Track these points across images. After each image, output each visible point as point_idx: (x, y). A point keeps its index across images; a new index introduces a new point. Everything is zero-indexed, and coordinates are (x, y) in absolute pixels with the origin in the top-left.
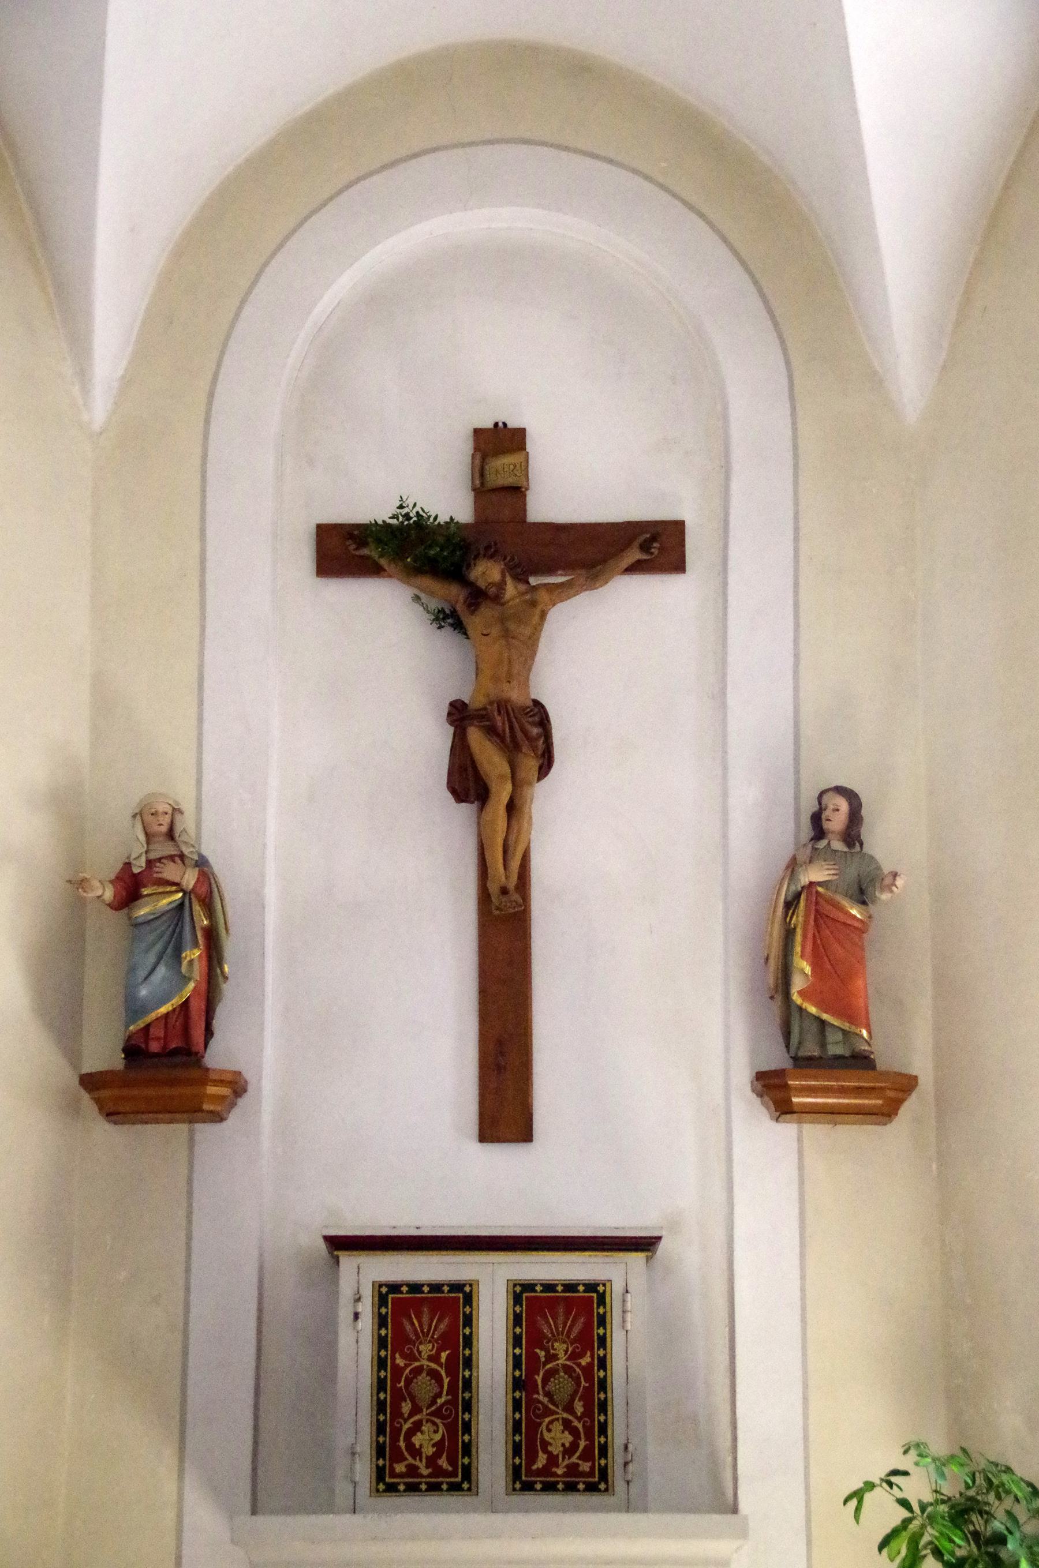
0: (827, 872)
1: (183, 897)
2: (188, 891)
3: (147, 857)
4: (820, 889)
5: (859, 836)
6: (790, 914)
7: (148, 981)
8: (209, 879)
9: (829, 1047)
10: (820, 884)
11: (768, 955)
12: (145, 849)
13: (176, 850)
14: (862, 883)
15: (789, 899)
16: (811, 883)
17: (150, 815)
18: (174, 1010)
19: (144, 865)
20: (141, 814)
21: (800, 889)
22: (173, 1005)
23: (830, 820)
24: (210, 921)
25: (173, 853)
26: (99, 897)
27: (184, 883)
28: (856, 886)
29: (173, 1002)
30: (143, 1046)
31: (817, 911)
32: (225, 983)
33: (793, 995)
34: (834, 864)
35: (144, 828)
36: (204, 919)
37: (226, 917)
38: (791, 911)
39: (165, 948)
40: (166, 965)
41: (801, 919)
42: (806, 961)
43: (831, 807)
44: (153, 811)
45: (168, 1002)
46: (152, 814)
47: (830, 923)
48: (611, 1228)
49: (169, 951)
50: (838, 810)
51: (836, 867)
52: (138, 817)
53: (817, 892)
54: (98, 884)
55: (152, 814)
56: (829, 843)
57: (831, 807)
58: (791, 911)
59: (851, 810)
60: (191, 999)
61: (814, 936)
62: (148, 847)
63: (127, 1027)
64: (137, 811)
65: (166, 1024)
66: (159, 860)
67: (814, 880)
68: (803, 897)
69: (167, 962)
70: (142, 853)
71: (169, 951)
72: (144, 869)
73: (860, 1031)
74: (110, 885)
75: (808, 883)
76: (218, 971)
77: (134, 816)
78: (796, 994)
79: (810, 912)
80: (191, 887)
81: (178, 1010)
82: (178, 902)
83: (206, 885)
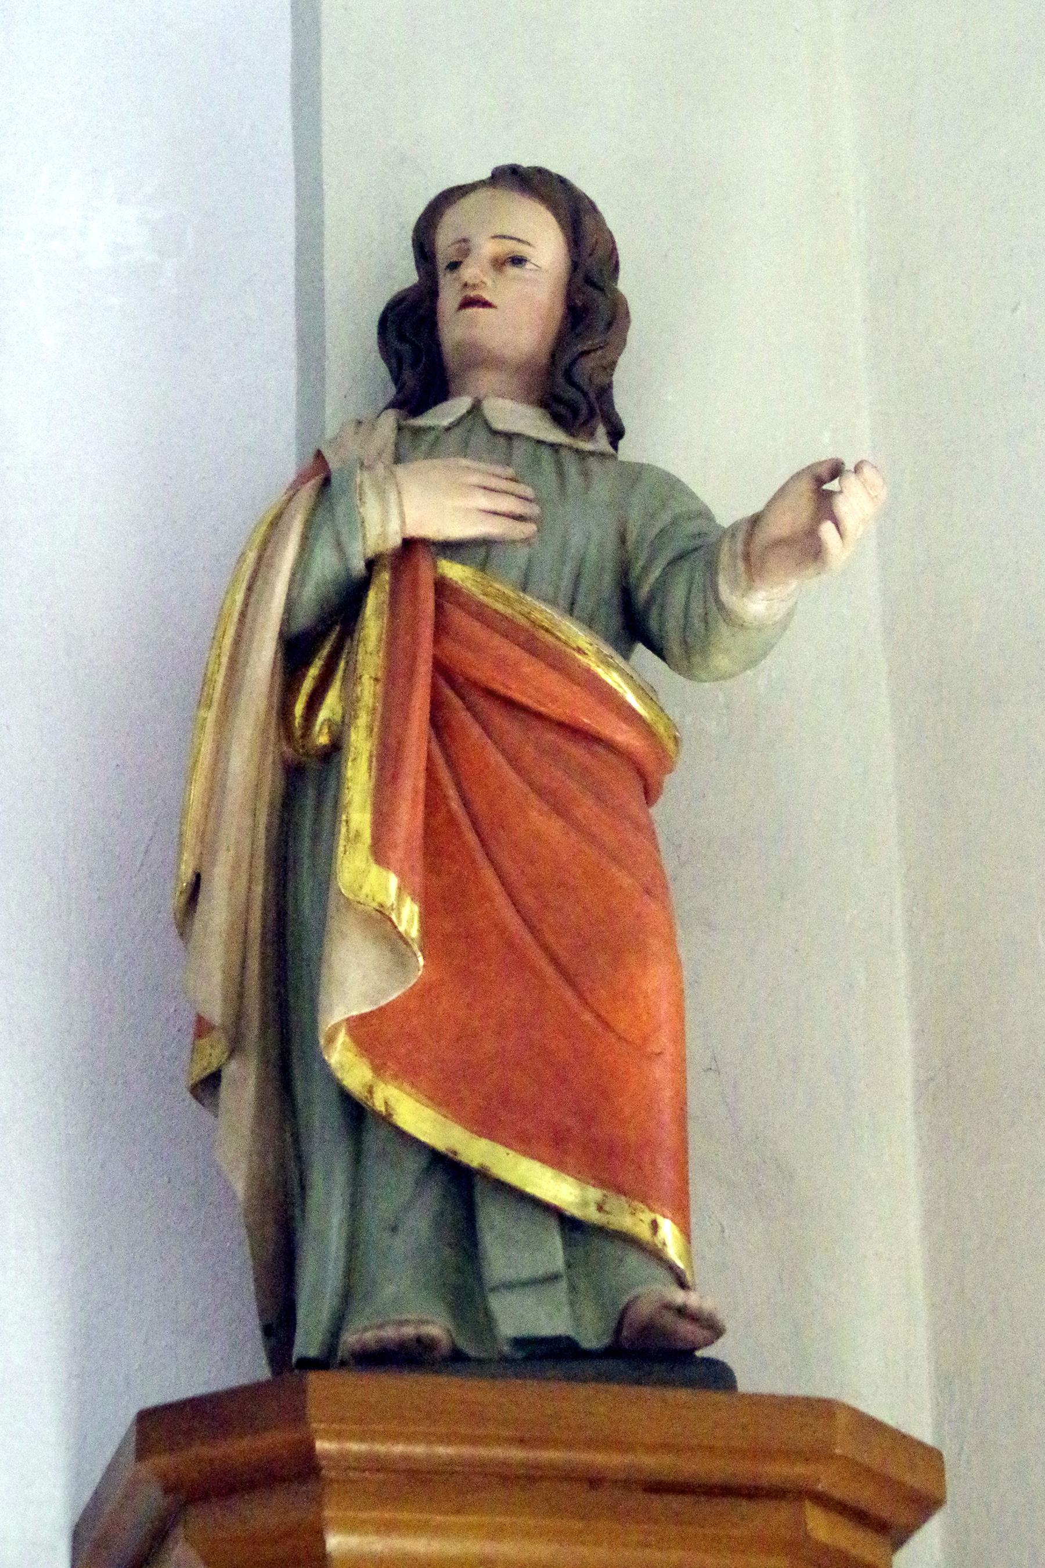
0: (485, 501)
4: (454, 571)
5: (605, 392)
6: (307, 686)
9: (497, 1304)
10: (452, 548)
11: (198, 877)
14: (632, 580)
15: (303, 620)
16: (410, 545)
21: (358, 566)
23: (486, 304)
28: (608, 579)
31: (442, 670)
33: (331, 1039)
34: (513, 480)
38: (314, 671)
41: (368, 691)
42: (400, 874)
43: (487, 248)
47: (499, 719)
48: (846, 1506)
50: (518, 261)
51: (529, 492)
53: (442, 587)
56: (476, 409)
57: (487, 248)
58: (314, 671)
59: (575, 266)
61: (430, 773)
67: (415, 530)
68: (374, 600)
73: (655, 1226)
75: (395, 541)
78: (342, 1037)
79: (411, 672)
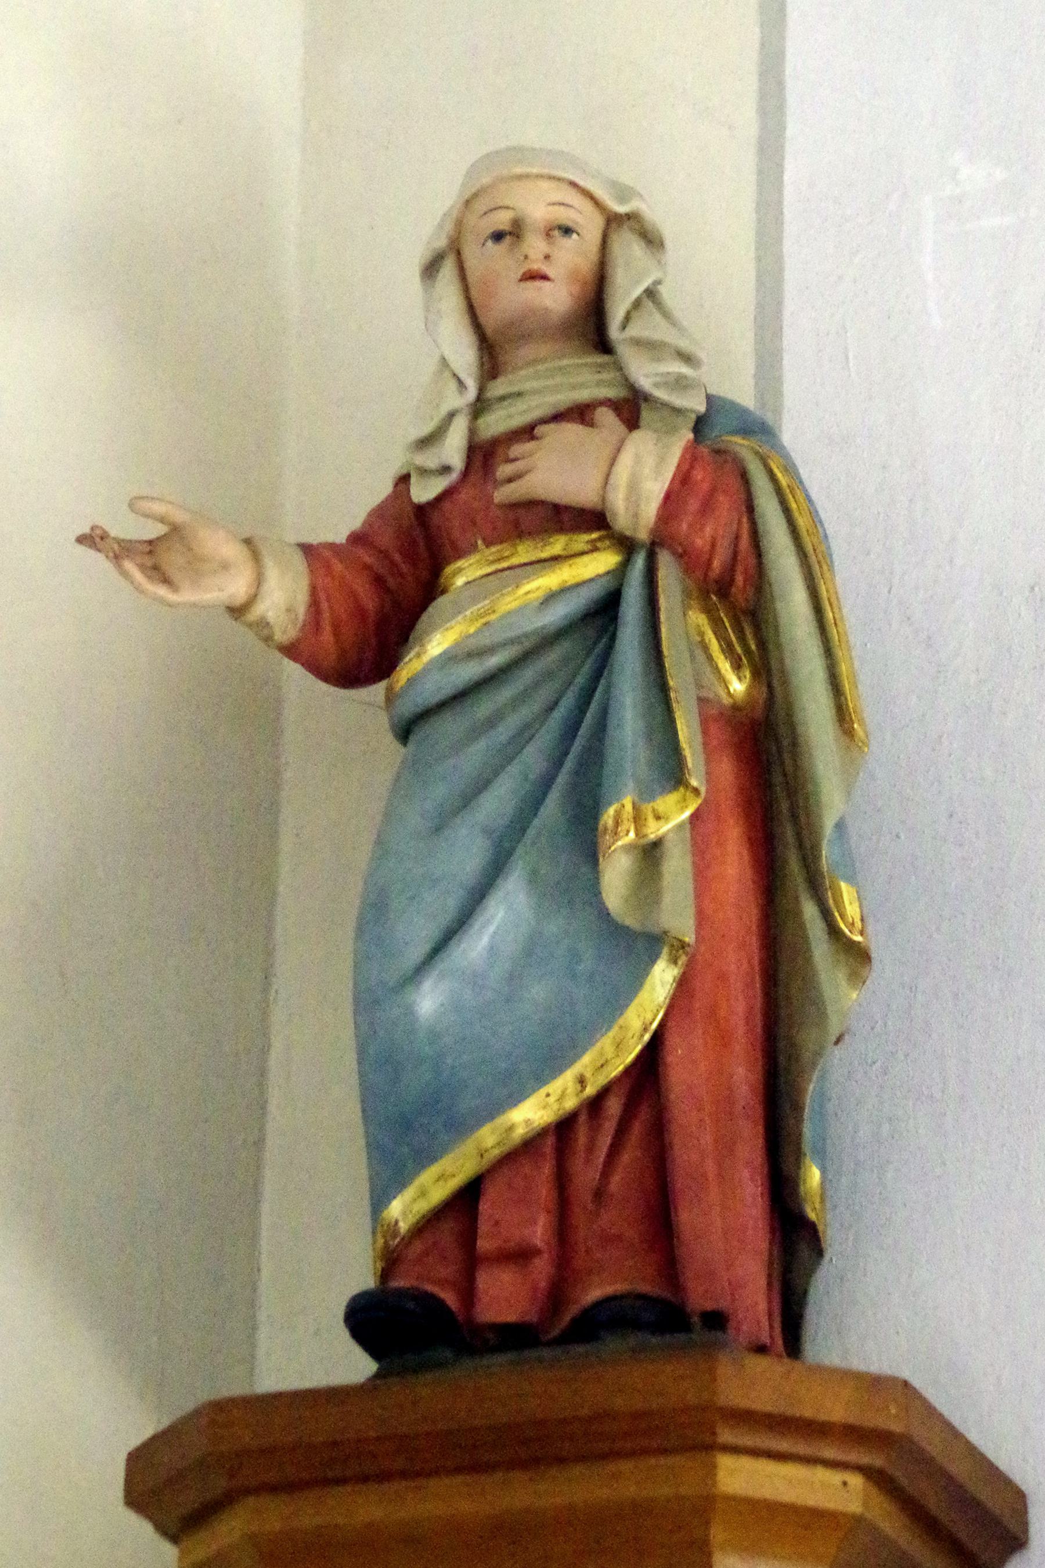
1: (621, 572)
2: (643, 535)
3: (472, 432)
7: (443, 964)
8: (744, 477)
12: (472, 393)
13: (610, 384)
17: (490, 243)
18: (595, 1105)
19: (457, 461)
20: (455, 249)
22: (582, 1081)
24: (756, 674)
25: (584, 395)
26: (237, 611)
27: (619, 506)
29: (585, 1062)
30: (450, 1298)
32: (856, 978)
35: (472, 312)
36: (725, 666)
37: (839, 653)
39: (534, 802)
40: (533, 878)
44: (502, 220)
45: (557, 1071)
46: (498, 236)
49: (553, 805)
52: (448, 270)
54: (231, 550)
55: (498, 236)
60: (676, 1053)
62: (481, 390)
63: (379, 1201)
64: (442, 243)
65: (562, 1180)
66: (528, 432)
69: (534, 872)
70: (451, 415)
71: (553, 805)
72: (454, 476)
74: (299, 562)
76: (809, 910)
77: (431, 269)
80: (650, 510)
81: (614, 1106)
82: (593, 593)
83: (726, 507)
